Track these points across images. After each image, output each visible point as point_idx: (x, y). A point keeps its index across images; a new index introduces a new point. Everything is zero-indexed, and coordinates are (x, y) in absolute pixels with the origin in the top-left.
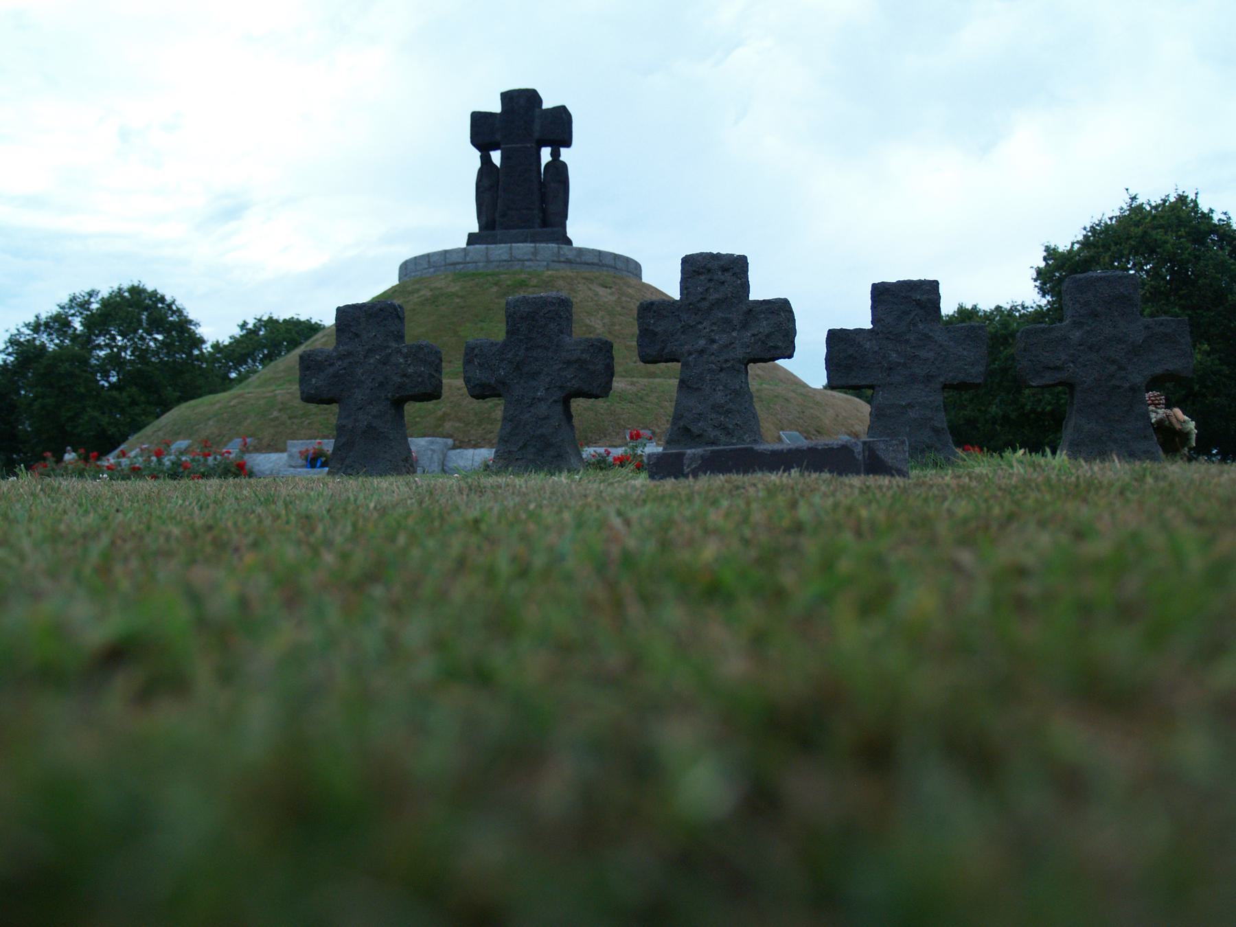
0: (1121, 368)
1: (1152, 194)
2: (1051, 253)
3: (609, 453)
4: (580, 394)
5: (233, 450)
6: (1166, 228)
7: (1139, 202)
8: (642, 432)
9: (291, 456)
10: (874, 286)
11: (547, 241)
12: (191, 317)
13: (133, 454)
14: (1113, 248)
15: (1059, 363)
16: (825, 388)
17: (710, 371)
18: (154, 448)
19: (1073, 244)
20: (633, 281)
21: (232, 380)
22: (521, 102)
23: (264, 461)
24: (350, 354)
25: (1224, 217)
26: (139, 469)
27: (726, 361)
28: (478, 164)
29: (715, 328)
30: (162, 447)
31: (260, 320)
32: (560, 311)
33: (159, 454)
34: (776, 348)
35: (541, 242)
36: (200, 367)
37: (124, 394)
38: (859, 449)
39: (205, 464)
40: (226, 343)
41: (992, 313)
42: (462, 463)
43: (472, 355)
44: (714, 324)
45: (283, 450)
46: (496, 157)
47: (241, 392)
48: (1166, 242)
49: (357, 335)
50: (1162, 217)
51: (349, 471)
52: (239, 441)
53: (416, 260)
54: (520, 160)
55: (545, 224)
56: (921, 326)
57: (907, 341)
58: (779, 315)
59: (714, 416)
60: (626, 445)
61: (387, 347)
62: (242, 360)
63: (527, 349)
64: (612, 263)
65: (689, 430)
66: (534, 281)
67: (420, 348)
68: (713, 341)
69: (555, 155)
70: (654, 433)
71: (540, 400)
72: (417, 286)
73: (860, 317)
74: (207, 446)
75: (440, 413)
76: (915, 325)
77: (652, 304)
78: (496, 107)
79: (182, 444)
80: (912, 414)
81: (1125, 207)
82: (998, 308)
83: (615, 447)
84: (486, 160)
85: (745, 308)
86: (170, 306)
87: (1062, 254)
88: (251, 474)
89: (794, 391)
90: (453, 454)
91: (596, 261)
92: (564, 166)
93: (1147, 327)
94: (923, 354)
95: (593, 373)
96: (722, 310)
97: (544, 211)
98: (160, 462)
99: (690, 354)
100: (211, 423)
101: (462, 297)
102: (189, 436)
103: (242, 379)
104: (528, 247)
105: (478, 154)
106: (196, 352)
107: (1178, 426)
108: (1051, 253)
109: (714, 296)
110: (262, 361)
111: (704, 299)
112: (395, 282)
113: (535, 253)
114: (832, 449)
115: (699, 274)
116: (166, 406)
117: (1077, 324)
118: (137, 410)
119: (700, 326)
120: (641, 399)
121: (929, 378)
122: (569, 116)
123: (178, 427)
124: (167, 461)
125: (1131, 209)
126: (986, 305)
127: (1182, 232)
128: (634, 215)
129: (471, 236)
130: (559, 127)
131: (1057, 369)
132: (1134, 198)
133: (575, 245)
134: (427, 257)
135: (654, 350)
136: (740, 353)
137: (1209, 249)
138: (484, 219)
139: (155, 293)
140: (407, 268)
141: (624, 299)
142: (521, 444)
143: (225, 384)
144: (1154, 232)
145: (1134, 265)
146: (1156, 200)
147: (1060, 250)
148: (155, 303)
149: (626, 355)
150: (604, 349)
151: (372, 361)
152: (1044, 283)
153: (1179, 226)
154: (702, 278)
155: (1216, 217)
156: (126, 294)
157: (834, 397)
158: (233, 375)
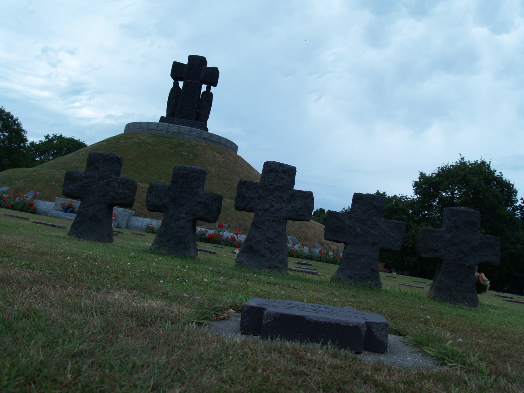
1: (471, 158)
2: (422, 176)
3: (207, 232)
5: (29, 196)
7: (465, 160)
8: (224, 224)
9: (56, 205)
10: (355, 194)
11: (197, 127)
12: (23, 128)
14: (450, 179)
19: (432, 174)
21: (36, 161)
22: (197, 62)
23: (43, 205)
25: (499, 174)
27: (277, 217)
29: (275, 200)
31: (55, 136)
32: (200, 176)
34: (302, 215)
35: (194, 127)
36: (23, 152)
40: (37, 143)
41: (392, 197)
42: (137, 223)
43: (152, 190)
44: (274, 198)
46: (181, 84)
48: (474, 181)
49: (97, 168)
50: (474, 169)
51: (79, 235)
52: (33, 192)
55: (197, 119)
60: (216, 229)
62: (43, 153)
66: (187, 145)
68: (272, 206)
69: (208, 89)
70: (229, 226)
72: (132, 136)
74: (17, 192)
77: (246, 182)
78: (185, 62)
81: (458, 162)
82: (395, 196)
84: (176, 85)
86: (14, 121)
87: (427, 178)
90: (134, 219)
91: (217, 141)
92: (211, 95)
93: (481, 239)
99: (260, 210)
100: (21, 181)
103: (41, 162)
105: (173, 81)
107: (482, 282)
108: (422, 176)
110: (52, 155)
111: (272, 185)
112: (122, 132)
114: (349, 327)
115: (272, 172)
119: (267, 198)
125: (461, 163)
126: (390, 193)
129: (162, 117)
130: (212, 76)
132: (463, 159)
133: (209, 131)
135: (243, 204)
137: (491, 187)
139: (9, 114)
140: (130, 127)
141: (227, 161)
143: (32, 163)
146: (472, 161)
147: (427, 175)
149: (228, 203)
150: (219, 199)
151: (102, 182)
154: (273, 174)
155: (496, 174)
157: (315, 224)
158: (37, 159)
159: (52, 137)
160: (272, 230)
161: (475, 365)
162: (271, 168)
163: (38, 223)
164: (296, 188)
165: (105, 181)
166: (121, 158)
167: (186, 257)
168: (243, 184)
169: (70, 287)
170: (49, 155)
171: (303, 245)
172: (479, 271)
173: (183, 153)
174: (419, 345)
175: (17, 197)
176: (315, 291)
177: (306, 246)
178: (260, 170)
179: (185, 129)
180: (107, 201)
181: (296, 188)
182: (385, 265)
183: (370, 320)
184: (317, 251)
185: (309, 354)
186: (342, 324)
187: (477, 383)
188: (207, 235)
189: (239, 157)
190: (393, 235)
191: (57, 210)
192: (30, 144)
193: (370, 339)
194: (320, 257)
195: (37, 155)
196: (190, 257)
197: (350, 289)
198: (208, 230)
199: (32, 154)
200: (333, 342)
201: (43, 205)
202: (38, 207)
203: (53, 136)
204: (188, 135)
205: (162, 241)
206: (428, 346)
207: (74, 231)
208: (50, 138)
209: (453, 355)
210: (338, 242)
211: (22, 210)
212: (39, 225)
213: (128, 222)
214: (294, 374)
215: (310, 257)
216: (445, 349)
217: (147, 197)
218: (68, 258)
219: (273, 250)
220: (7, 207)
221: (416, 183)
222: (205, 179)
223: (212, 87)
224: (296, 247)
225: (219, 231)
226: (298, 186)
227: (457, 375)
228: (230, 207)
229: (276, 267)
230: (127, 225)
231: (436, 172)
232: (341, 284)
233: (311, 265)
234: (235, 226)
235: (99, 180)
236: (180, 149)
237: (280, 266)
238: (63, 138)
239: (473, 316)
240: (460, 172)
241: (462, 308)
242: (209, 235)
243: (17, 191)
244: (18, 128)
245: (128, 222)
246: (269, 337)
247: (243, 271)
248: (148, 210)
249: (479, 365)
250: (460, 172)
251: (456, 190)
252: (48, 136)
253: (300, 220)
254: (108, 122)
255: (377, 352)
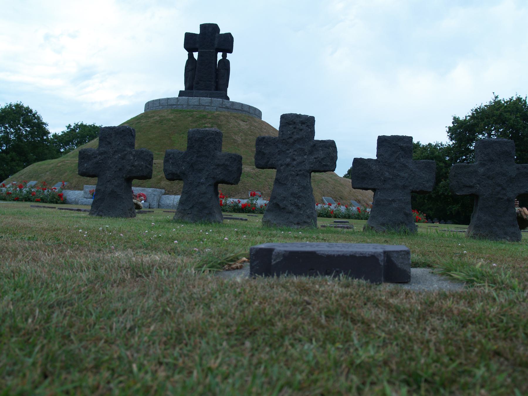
0: (503, 189)
1: (505, 96)
2: (456, 120)
3: (239, 202)
4: (223, 182)
5: (57, 187)
6: (511, 112)
7: (499, 99)
8: (256, 192)
9: (85, 193)
10: (379, 137)
11: (218, 97)
13: (8, 186)
14: (485, 120)
15: (472, 184)
16: (345, 176)
17: (291, 175)
18: (19, 184)
19: (466, 117)
20: (257, 119)
22: (210, 30)
23: (72, 194)
24: (105, 152)
26: (11, 193)
27: (300, 170)
28: (187, 58)
30: (23, 184)
31: (77, 125)
32: (216, 138)
33: (21, 187)
34: (326, 165)
35: (214, 97)
36: (47, 145)
37: (9, 156)
38: (381, 258)
39: (43, 194)
40: (60, 135)
41: (426, 146)
42: (168, 202)
43: (168, 158)
45: (82, 190)
46: (196, 55)
47: (64, 159)
48: (510, 119)
49: (110, 143)
50: (509, 107)
51: (101, 213)
53: (153, 102)
54: (208, 57)
55: (217, 89)
56: (402, 160)
57: (395, 167)
58: (329, 148)
59: (292, 199)
60: (248, 198)
61: (125, 150)
62: (67, 143)
63: (197, 157)
64: (248, 110)
65: (278, 205)
66: (210, 116)
67: (142, 152)
68: (294, 160)
69: (224, 56)
70: (262, 194)
71: (202, 184)
72: (153, 114)
73: (370, 153)
74: (45, 185)
75: (159, 177)
76: (399, 159)
77: (264, 138)
79: (33, 183)
80: (394, 205)
81: (492, 101)
82: (430, 144)
83: (243, 199)
84: (191, 56)
85: (312, 144)
86: (34, 115)
87: (461, 121)
88: (65, 202)
89: (331, 178)
91: (240, 108)
92: (228, 62)
93: (518, 169)
94: (402, 174)
95: (231, 173)
96: (298, 143)
97: (217, 83)
98: (21, 191)
99: (282, 166)
100: (48, 173)
101: (174, 121)
102: (36, 179)
103: (66, 152)
104: (208, 99)
105: (187, 53)
106: (45, 138)
108: (456, 120)
109: (296, 137)
113: (211, 102)
114: (365, 257)
115: (289, 124)
116: (29, 163)
117: (482, 165)
118: (14, 163)
119: (288, 152)
120: (257, 176)
121: (404, 187)
122: (232, 38)
123: (31, 175)
124: (24, 191)
125: (495, 102)
127: (518, 115)
128: (260, 87)
129: (181, 92)
130: (227, 43)
131: (471, 187)
132: (496, 97)
134: (159, 100)
135: (263, 162)
136: (308, 167)
138: (188, 84)
139: (28, 108)
140: (149, 105)
141: (252, 128)
142: (191, 206)
143: (58, 154)
144: (505, 114)
145: (495, 129)
146: (507, 99)
147: (461, 119)
148: (27, 113)
150: (238, 160)
151: (116, 157)
152: (452, 134)
153: (517, 112)
154: (291, 126)
156: (13, 107)
158: (62, 150)
159: (74, 127)
160: (297, 184)
161: (506, 282)
162: (287, 120)
163: (63, 209)
164: (317, 138)
165: (120, 155)
166: (133, 129)
167: (211, 223)
168: (262, 141)
169: (69, 250)
170: (73, 144)
171: (339, 204)
172: (521, 206)
173: (206, 125)
174: (447, 273)
175: (45, 189)
176: (345, 240)
177: (343, 205)
178: (276, 124)
179: (206, 100)
180: (124, 175)
181: (317, 138)
182: (426, 216)
183: (390, 248)
184: (355, 209)
185: (317, 286)
186: (358, 255)
187: (507, 297)
188: (240, 205)
189: (265, 123)
190: (424, 175)
191: (87, 198)
192: (53, 136)
193: (391, 269)
194: (358, 215)
195: (61, 146)
196: (215, 222)
197: (384, 236)
198: (240, 200)
199: (56, 146)
200: (346, 274)
201: (72, 194)
202: (68, 198)
203: (74, 125)
204: (208, 106)
205: (185, 210)
206: (456, 271)
207: (95, 210)
208: (72, 127)
209: (483, 276)
210: (367, 189)
211: (51, 202)
212: (64, 210)
213: (159, 201)
214: (295, 304)
215: (348, 216)
216: (473, 271)
217: (165, 166)
218: (80, 231)
219: (300, 205)
220: (37, 201)
221: (450, 128)
222: (222, 141)
223: (228, 54)
224: (332, 207)
225: (252, 200)
226: (319, 136)
227: (484, 292)
228: (260, 175)
229: (305, 222)
230: (159, 204)
231: (470, 114)
232: (374, 232)
233: (348, 222)
234: (258, 185)
235: (113, 155)
236: (203, 122)
237: (308, 221)
238: (85, 126)
239: (515, 249)
240: (495, 111)
241: (505, 243)
242: (242, 205)
243: (44, 183)
244: (38, 122)
245: (159, 201)
246: (275, 274)
247: (270, 230)
248: (167, 179)
249: (511, 282)
250: (495, 111)
251: (493, 130)
252: (70, 126)
253: (325, 171)
254: (124, 103)
255: (400, 283)
